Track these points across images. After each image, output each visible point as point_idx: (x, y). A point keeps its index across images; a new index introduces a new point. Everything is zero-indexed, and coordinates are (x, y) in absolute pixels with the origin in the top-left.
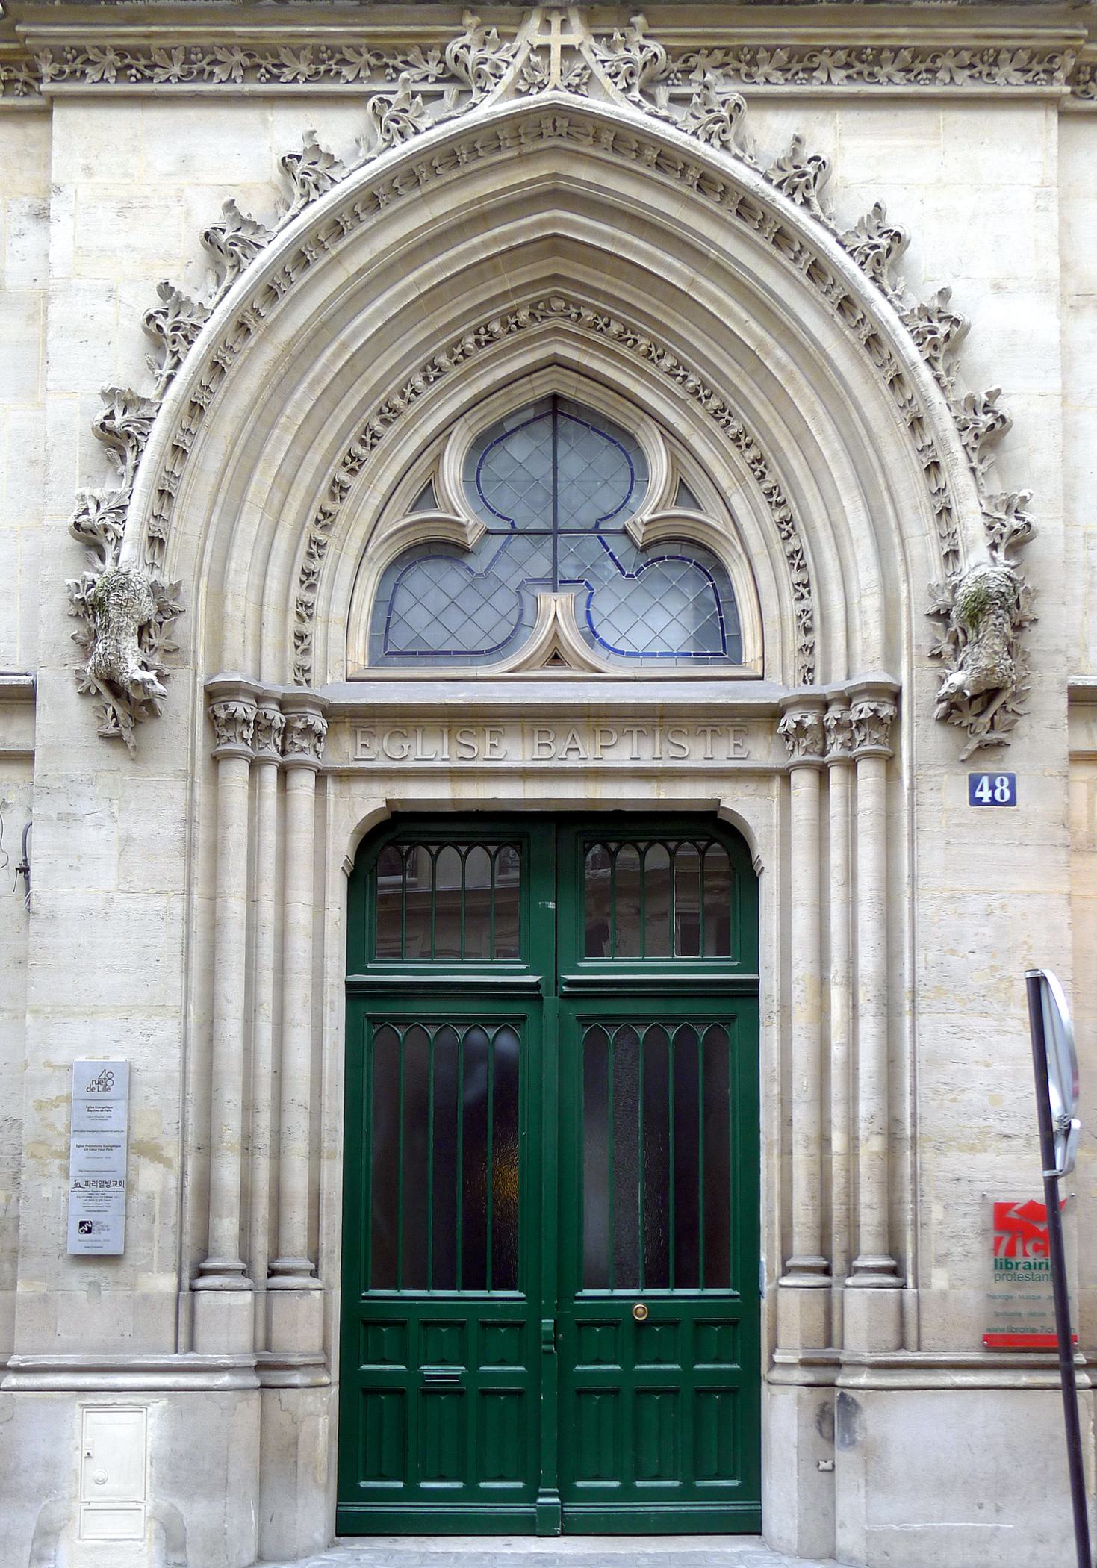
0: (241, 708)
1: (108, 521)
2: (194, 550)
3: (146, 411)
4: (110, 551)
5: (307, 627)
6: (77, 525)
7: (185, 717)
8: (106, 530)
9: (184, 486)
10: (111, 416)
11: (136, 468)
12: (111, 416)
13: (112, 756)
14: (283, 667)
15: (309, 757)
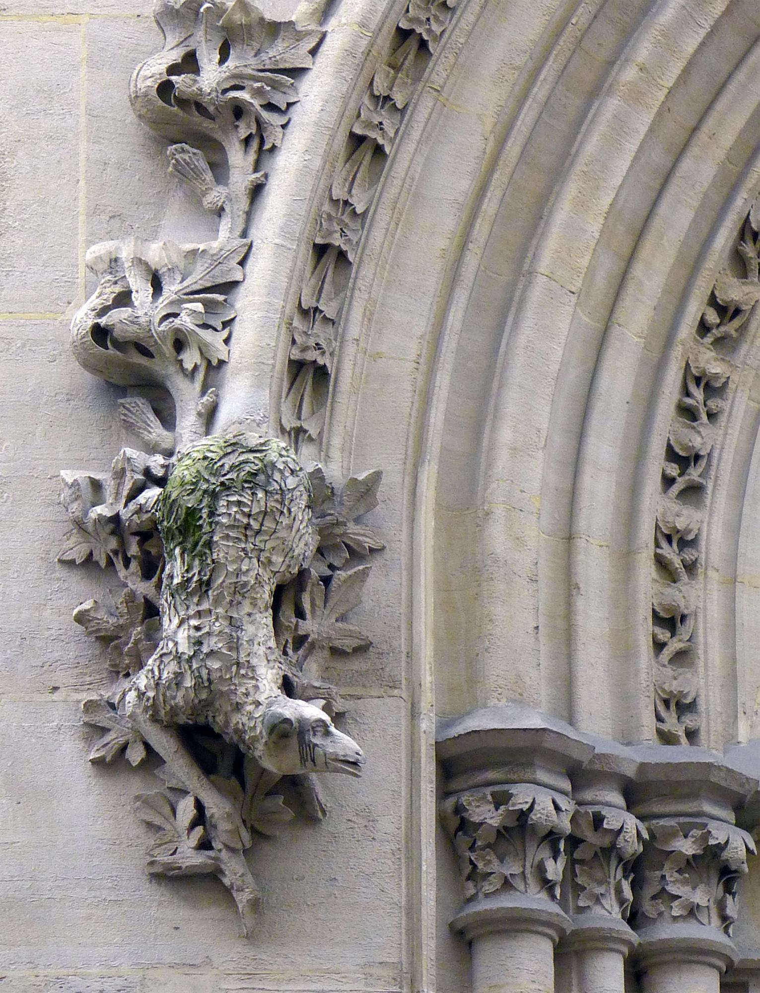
0: (544, 800)
1: (185, 321)
2: (404, 399)
3: (280, 52)
4: (188, 399)
5: (686, 595)
6: (100, 334)
7: (390, 823)
8: (179, 345)
9: (377, 236)
10: (189, 63)
11: (257, 191)
12: (189, 63)
13: (195, 927)
14: (623, 697)
15: (708, 931)
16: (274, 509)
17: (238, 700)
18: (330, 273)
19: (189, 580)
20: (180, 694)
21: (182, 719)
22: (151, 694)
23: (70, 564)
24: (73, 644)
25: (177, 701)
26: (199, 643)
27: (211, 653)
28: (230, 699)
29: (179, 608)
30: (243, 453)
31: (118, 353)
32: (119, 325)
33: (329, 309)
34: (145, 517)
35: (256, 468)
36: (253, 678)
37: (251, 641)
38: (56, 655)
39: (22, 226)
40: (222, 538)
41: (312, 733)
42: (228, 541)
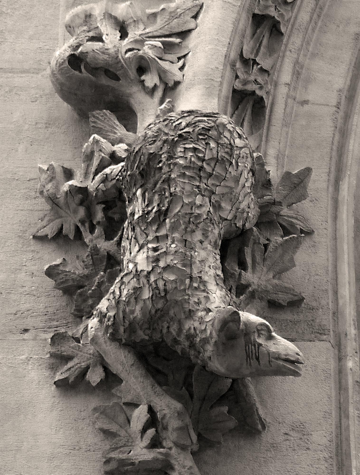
1: (148, 51)
6: (75, 60)
16: (225, 159)
17: (191, 308)
18: (265, 42)
19: (148, 213)
20: (138, 308)
21: (141, 335)
22: (111, 314)
23: (40, 239)
24: (43, 298)
25: (135, 315)
26: (157, 260)
27: (167, 268)
28: (183, 308)
29: (139, 238)
30: (197, 117)
31: (90, 76)
32: (92, 53)
33: (265, 62)
34: (110, 184)
35: (209, 125)
36: (204, 291)
37: (202, 261)
38: (28, 306)
39: (13, 13)
40: (179, 176)
41: (256, 335)
42: (184, 179)
